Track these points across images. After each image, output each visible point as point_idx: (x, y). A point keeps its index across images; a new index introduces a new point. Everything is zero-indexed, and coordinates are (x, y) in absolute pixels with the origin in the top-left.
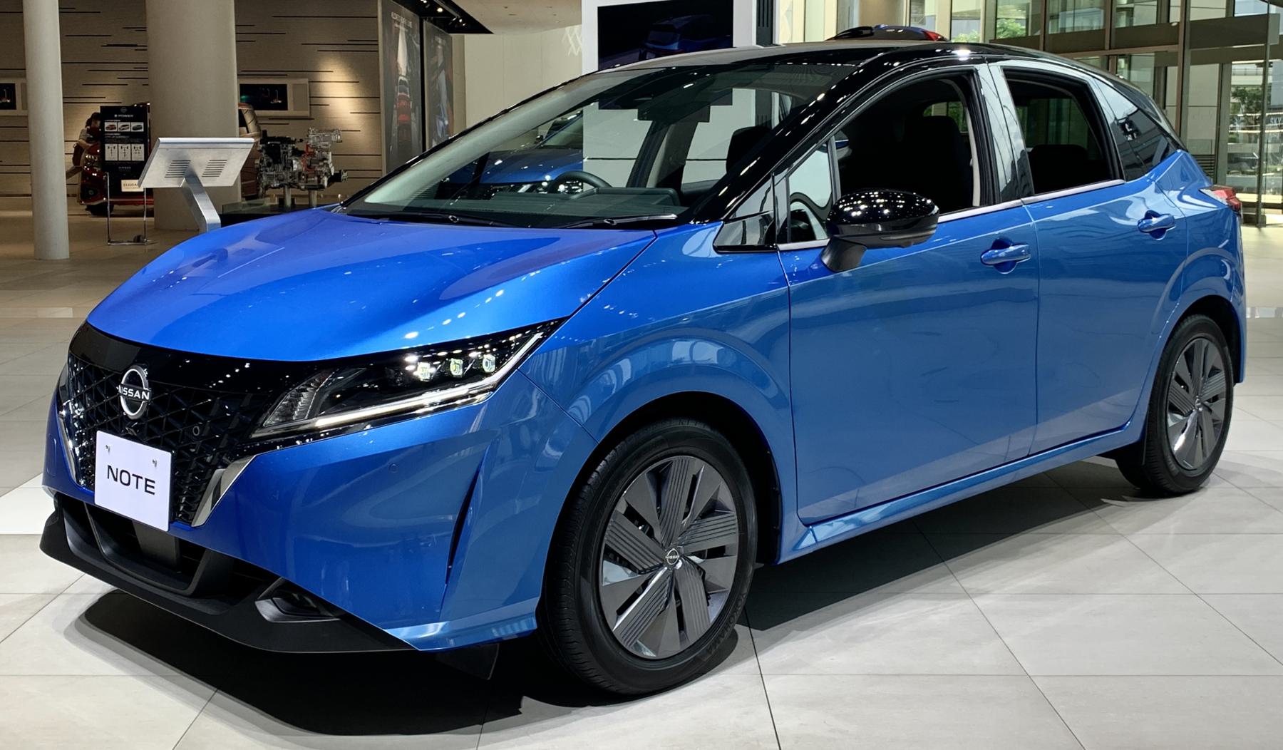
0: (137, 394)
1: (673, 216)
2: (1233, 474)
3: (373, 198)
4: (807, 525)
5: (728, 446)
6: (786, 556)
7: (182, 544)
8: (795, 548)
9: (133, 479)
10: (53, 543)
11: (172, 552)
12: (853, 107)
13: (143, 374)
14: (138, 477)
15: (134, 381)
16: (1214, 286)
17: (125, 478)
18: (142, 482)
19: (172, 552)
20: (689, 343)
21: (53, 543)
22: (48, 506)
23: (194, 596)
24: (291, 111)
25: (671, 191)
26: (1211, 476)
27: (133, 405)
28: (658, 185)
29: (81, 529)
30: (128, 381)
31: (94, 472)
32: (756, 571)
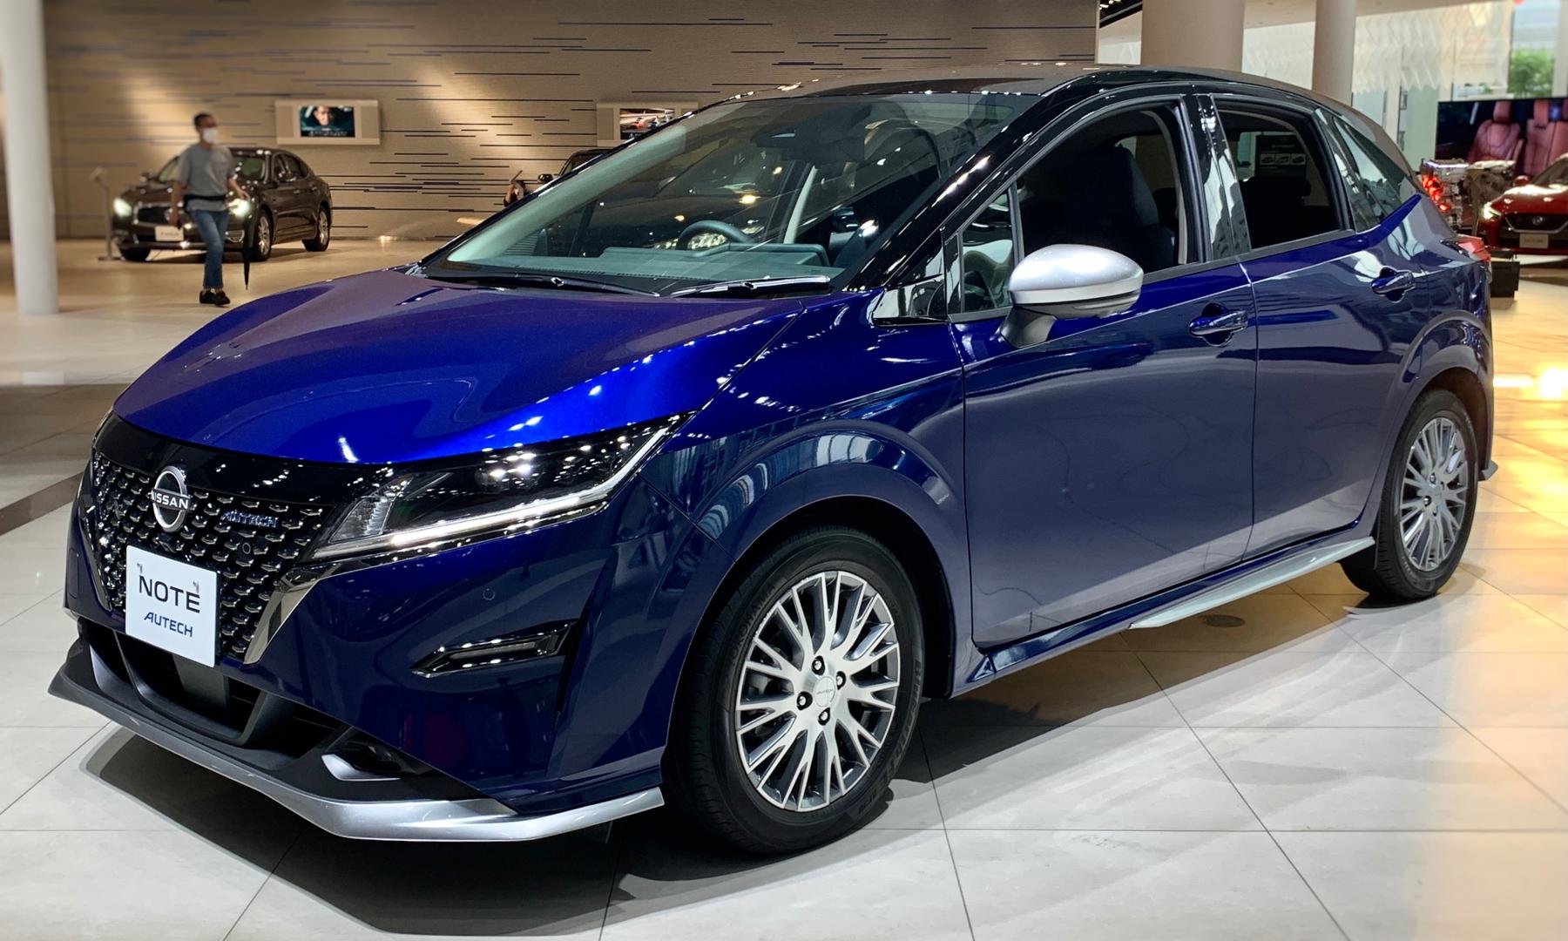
0: (174, 502)
1: (822, 279)
2: (1469, 566)
3: (457, 257)
4: (982, 651)
5: (886, 551)
6: (960, 688)
7: (233, 686)
8: (970, 680)
9: (172, 593)
10: (73, 680)
11: (219, 691)
12: (1037, 147)
13: (180, 475)
14: (178, 591)
15: (169, 513)
16: (1463, 354)
17: (161, 591)
18: (182, 597)
19: (219, 691)
20: (849, 438)
21: (73, 680)
22: (69, 630)
23: (245, 746)
24: (358, 139)
25: (819, 247)
26: (1455, 575)
27: (169, 513)
28: (798, 240)
29: (109, 658)
30: (161, 486)
31: (124, 606)
32: (922, 706)
